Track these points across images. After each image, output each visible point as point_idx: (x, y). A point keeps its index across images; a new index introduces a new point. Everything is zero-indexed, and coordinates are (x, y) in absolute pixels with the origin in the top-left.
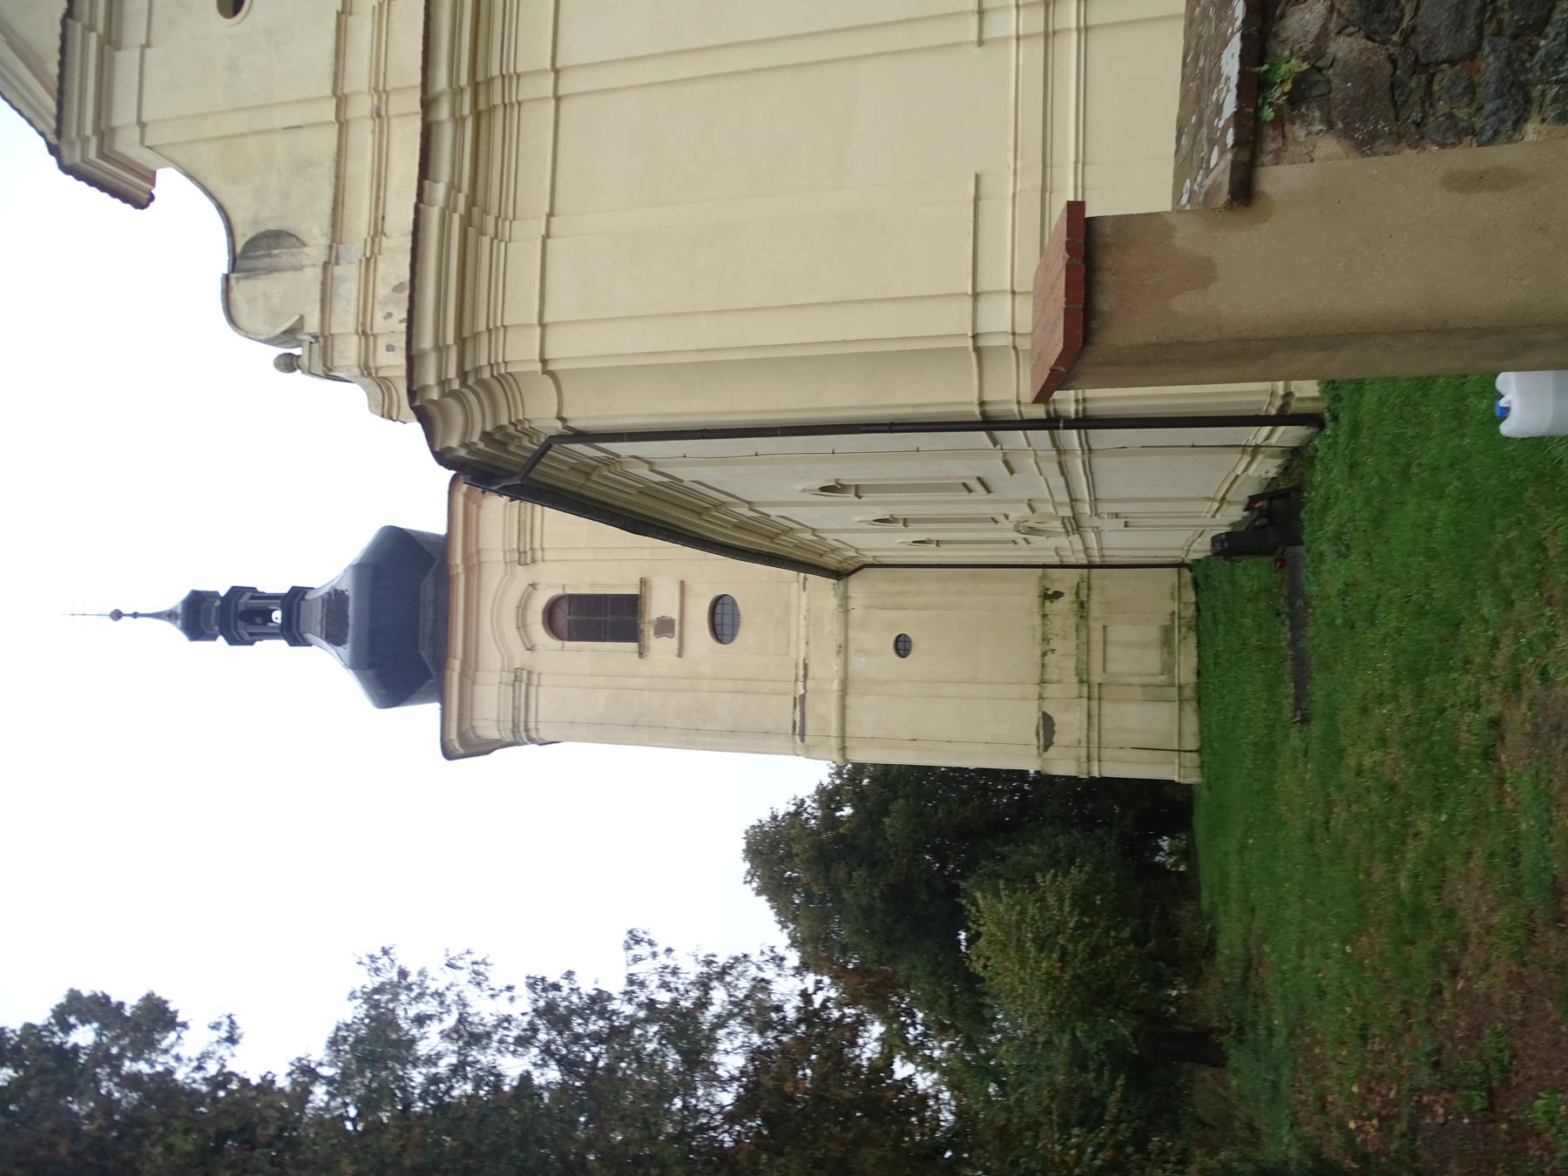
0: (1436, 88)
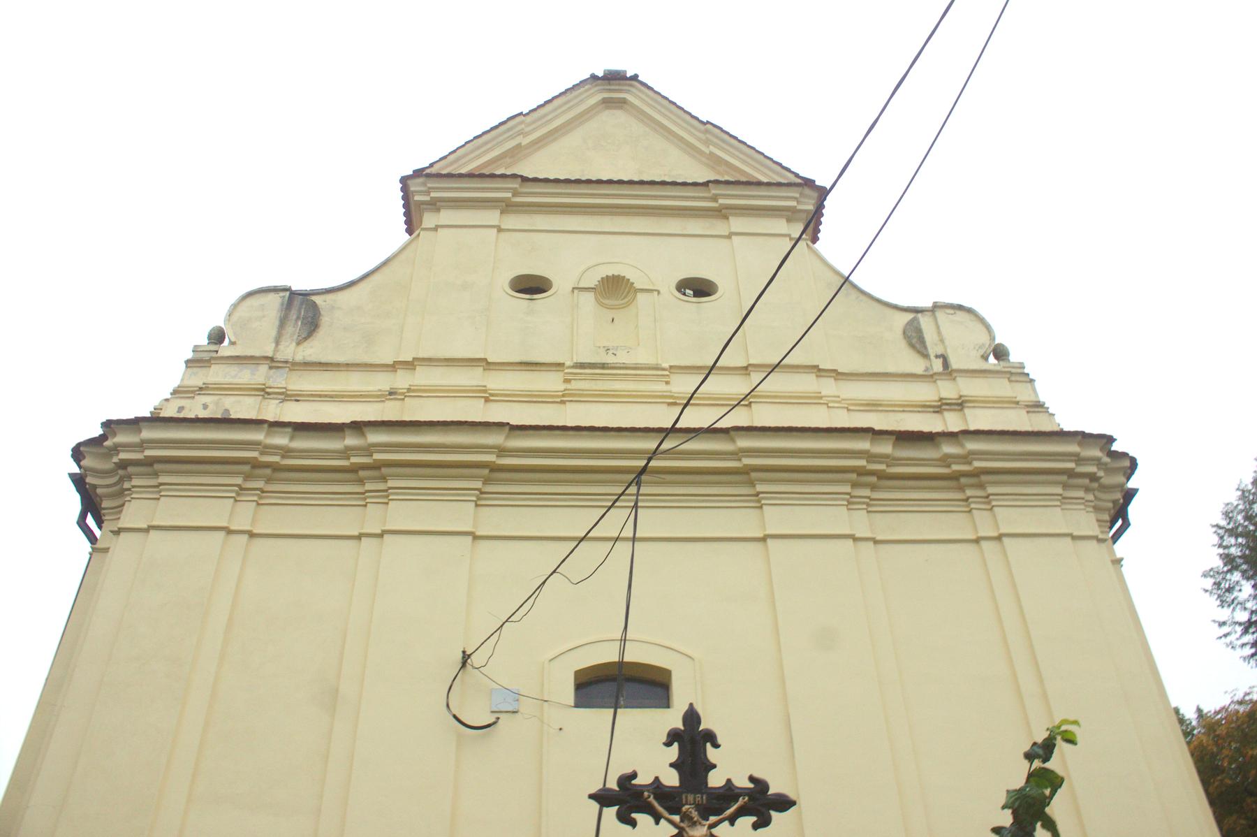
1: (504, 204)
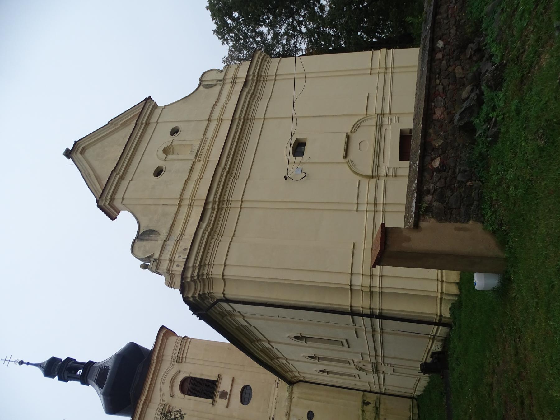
0: (453, 213)
1: (120, 179)
